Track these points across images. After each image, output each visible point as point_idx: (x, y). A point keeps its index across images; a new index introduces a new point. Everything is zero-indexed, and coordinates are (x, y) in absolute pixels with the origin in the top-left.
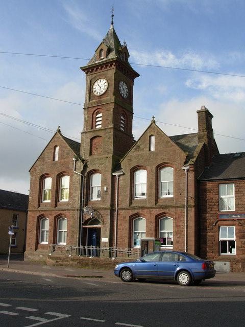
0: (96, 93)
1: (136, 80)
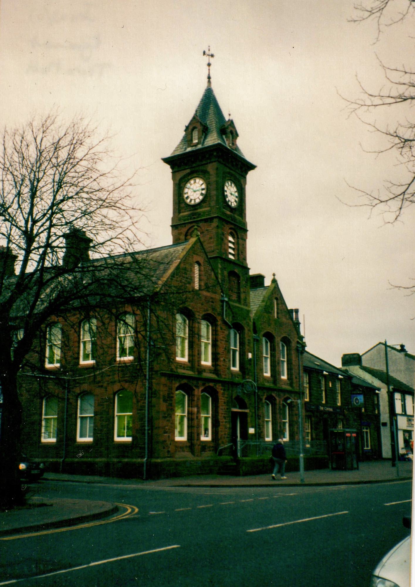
0: (188, 201)
1: (251, 176)
